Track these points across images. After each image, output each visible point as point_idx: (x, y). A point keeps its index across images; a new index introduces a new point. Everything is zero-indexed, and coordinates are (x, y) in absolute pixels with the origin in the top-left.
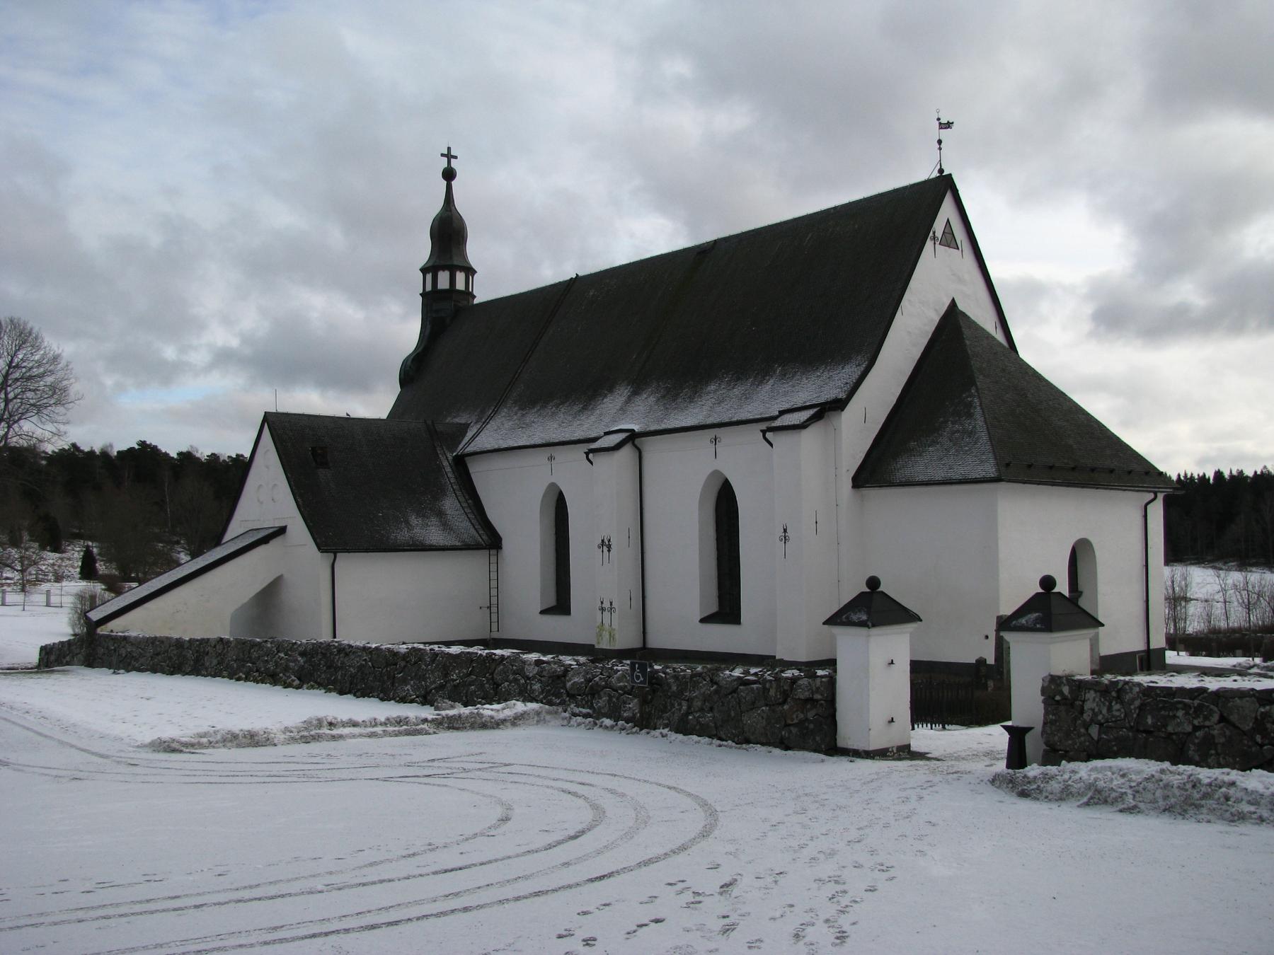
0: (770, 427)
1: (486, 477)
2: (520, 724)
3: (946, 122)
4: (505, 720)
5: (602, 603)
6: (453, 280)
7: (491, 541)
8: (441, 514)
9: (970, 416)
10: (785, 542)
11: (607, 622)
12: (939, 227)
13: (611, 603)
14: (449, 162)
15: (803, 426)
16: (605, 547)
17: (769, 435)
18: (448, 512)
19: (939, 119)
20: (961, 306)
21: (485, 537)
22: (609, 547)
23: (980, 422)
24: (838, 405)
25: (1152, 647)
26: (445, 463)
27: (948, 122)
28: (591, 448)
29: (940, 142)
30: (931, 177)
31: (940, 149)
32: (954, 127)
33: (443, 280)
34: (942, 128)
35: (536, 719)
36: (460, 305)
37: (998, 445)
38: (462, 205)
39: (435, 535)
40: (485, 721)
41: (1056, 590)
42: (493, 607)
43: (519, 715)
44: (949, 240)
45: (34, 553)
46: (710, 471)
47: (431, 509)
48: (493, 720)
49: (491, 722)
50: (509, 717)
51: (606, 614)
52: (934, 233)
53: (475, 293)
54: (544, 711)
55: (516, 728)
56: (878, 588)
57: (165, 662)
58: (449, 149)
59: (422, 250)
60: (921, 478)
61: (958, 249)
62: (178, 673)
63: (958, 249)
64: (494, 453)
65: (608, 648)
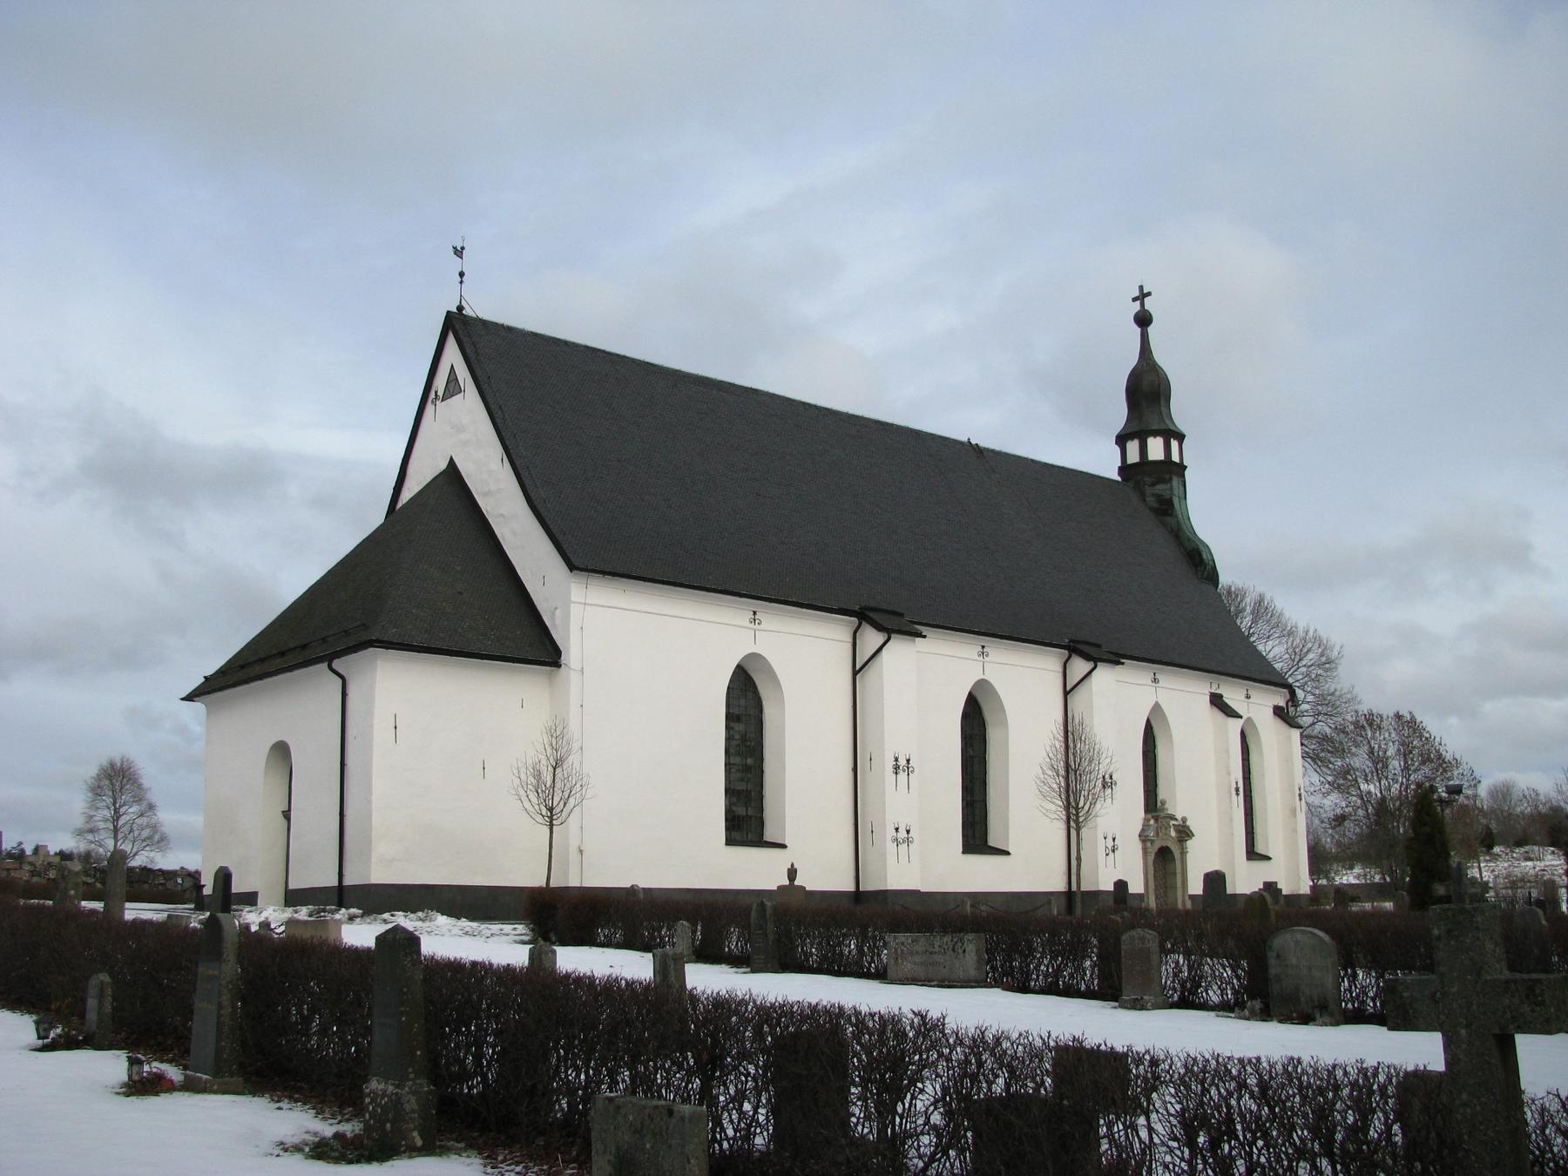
13: (908, 761)
14: (1142, 305)
25: (348, 882)
29: (462, 274)
31: (461, 282)
33: (1133, 447)
38: (1160, 357)
45: (1402, 783)
46: (276, 740)
52: (436, 392)
53: (1185, 464)
57: (1410, 775)
59: (1118, 414)
62: (998, 987)
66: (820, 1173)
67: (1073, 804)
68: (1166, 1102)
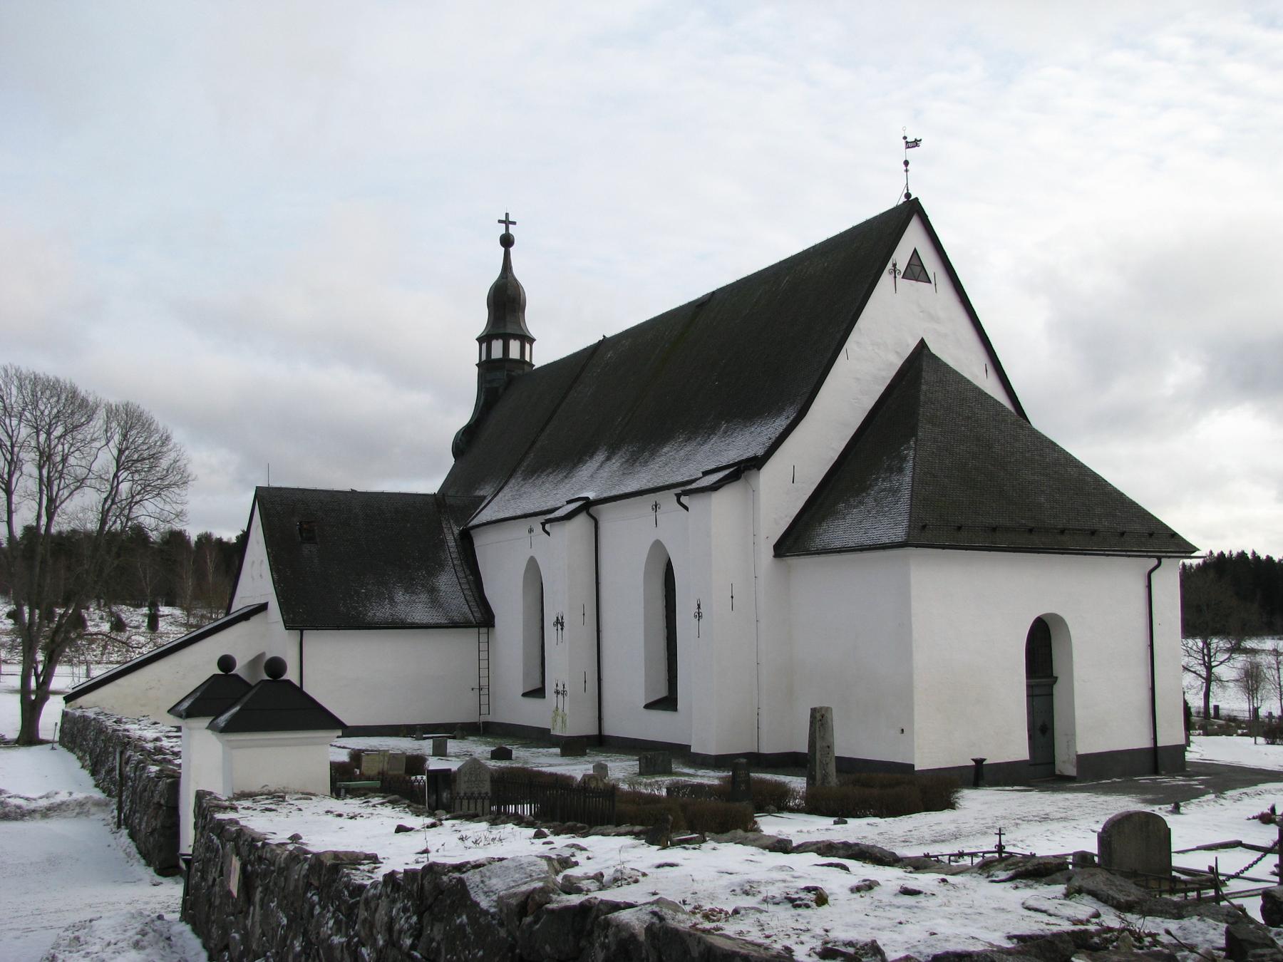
0: (685, 491)
1: (489, 549)
2: (53, 816)
3: (914, 140)
4: (34, 811)
5: (557, 685)
6: (506, 349)
7: (484, 619)
8: (433, 591)
9: (901, 470)
10: (699, 620)
11: (560, 706)
12: (901, 256)
14: (507, 228)
15: (715, 487)
16: (559, 625)
17: (684, 499)
18: (443, 588)
19: (905, 138)
20: (934, 348)
21: (478, 615)
22: (562, 625)
23: (907, 478)
24: (756, 463)
26: (450, 538)
27: (916, 140)
28: (548, 518)
29: (906, 163)
30: (899, 204)
31: (907, 171)
32: (921, 144)
33: (497, 349)
34: (909, 147)
35: (76, 811)
36: (513, 373)
37: (919, 502)
38: (518, 271)
39: (420, 613)
40: (9, 811)
41: (284, 677)
42: (483, 690)
43: (55, 805)
44: (916, 271)
47: (423, 586)
48: (18, 811)
49: (16, 813)
50: (41, 807)
51: (560, 696)
52: (895, 265)
53: (533, 363)
54: (90, 802)
55: (47, 820)
56: (282, 676)
58: (507, 215)
59: (479, 319)
60: (838, 544)
61: (930, 282)
63: (930, 282)
64: (488, 526)
65: (560, 734)
66: (434, 944)
67: (44, 487)
68: (101, 414)
